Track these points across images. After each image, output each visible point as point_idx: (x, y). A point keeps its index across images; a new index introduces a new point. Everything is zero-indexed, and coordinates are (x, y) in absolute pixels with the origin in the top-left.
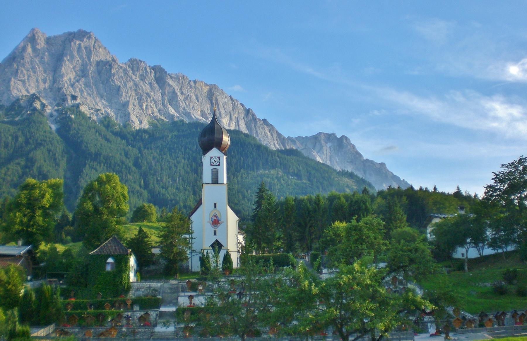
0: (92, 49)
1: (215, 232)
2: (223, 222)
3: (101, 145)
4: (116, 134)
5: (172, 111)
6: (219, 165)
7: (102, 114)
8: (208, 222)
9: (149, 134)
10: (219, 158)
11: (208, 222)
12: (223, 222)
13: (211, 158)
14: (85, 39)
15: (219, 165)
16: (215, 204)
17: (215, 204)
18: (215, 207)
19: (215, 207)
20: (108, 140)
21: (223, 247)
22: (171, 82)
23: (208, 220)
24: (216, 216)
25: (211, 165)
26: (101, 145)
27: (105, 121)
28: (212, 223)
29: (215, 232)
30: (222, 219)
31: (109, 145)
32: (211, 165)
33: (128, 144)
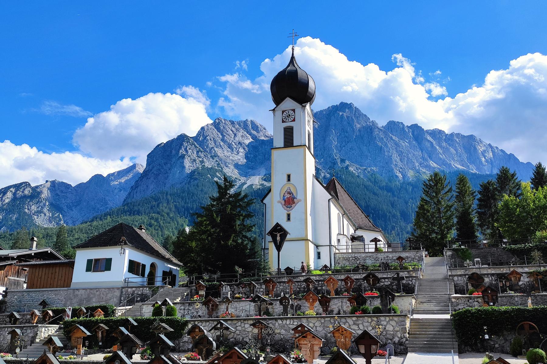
0: (354, 118)
1: (289, 215)
2: (300, 201)
3: (369, 198)
4: (381, 188)
5: (433, 164)
6: (294, 120)
7: (369, 172)
8: (279, 202)
9: (412, 185)
10: (294, 110)
11: (279, 202)
12: (300, 201)
13: (283, 112)
14: (347, 110)
15: (294, 120)
16: (289, 176)
17: (289, 176)
18: (289, 180)
19: (289, 180)
20: (375, 194)
21: (288, 237)
22: (429, 138)
23: (279, 199)
24: (290, 193)
25: (283, 122)
26: (369, 198)
27: (372, 177)
28: (283, 202)
29: (289, 215)
30: (299, 197)
31: (377, 197)
32: (283, 122)
33: (394, 195)
